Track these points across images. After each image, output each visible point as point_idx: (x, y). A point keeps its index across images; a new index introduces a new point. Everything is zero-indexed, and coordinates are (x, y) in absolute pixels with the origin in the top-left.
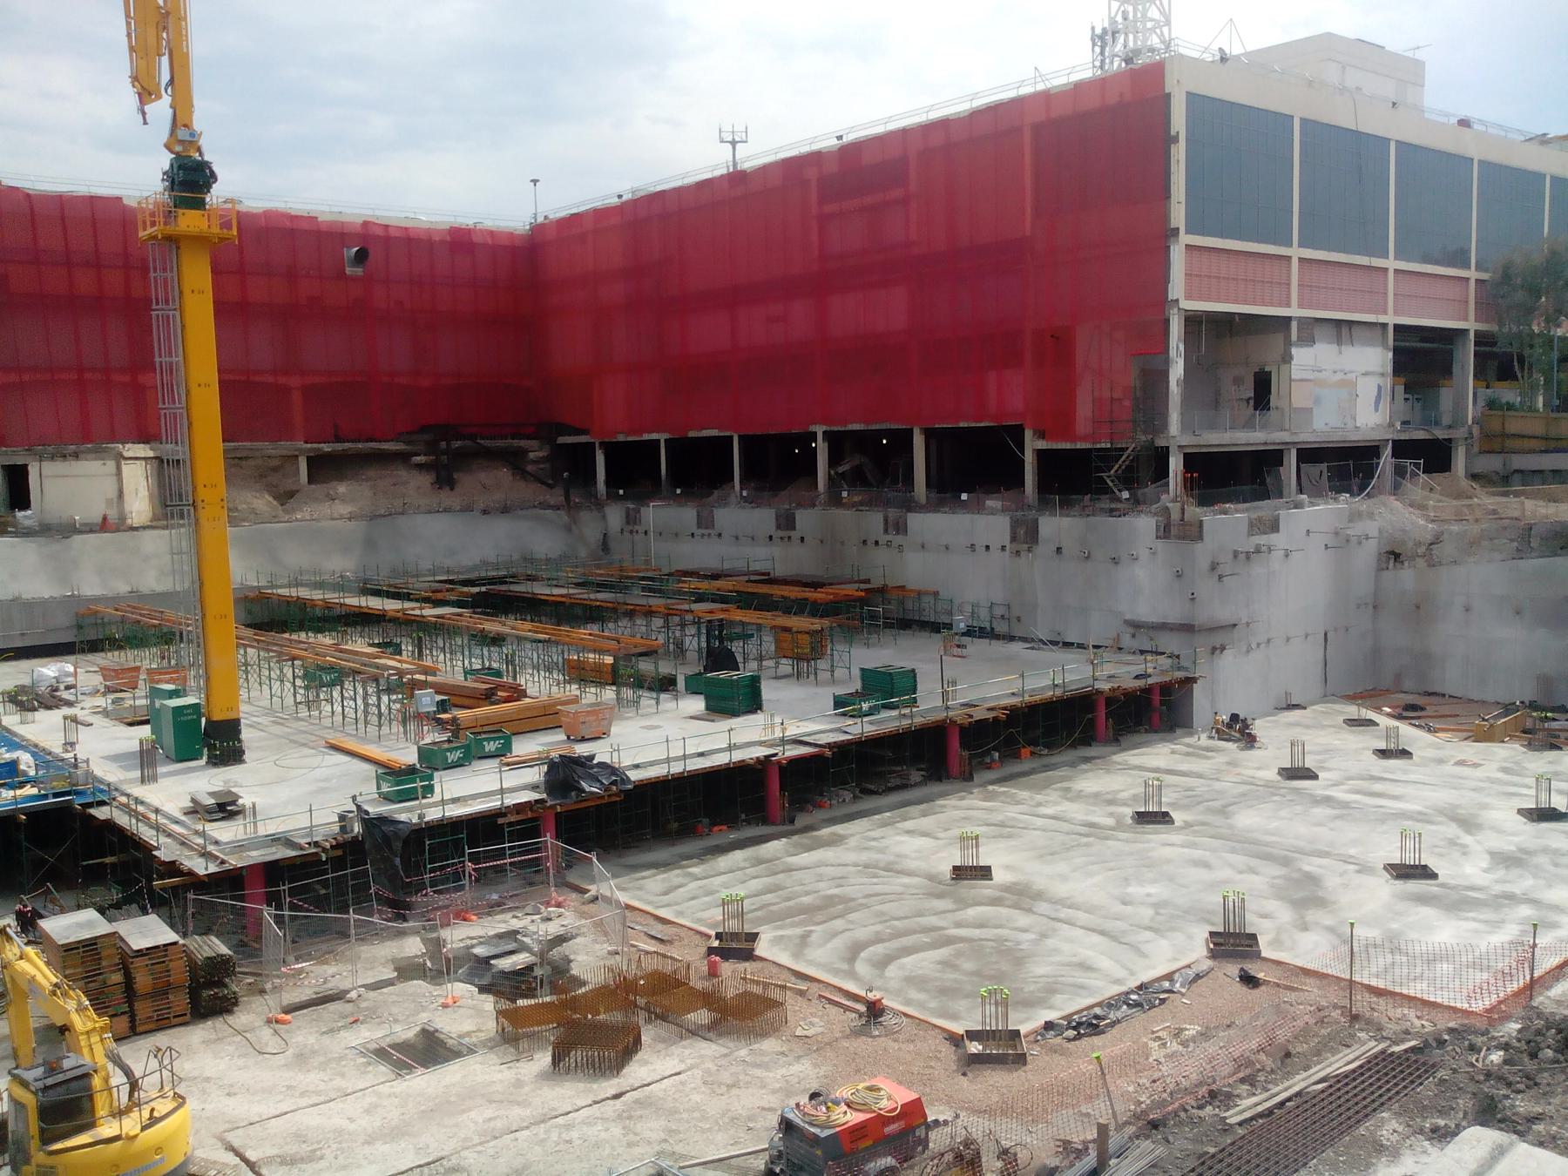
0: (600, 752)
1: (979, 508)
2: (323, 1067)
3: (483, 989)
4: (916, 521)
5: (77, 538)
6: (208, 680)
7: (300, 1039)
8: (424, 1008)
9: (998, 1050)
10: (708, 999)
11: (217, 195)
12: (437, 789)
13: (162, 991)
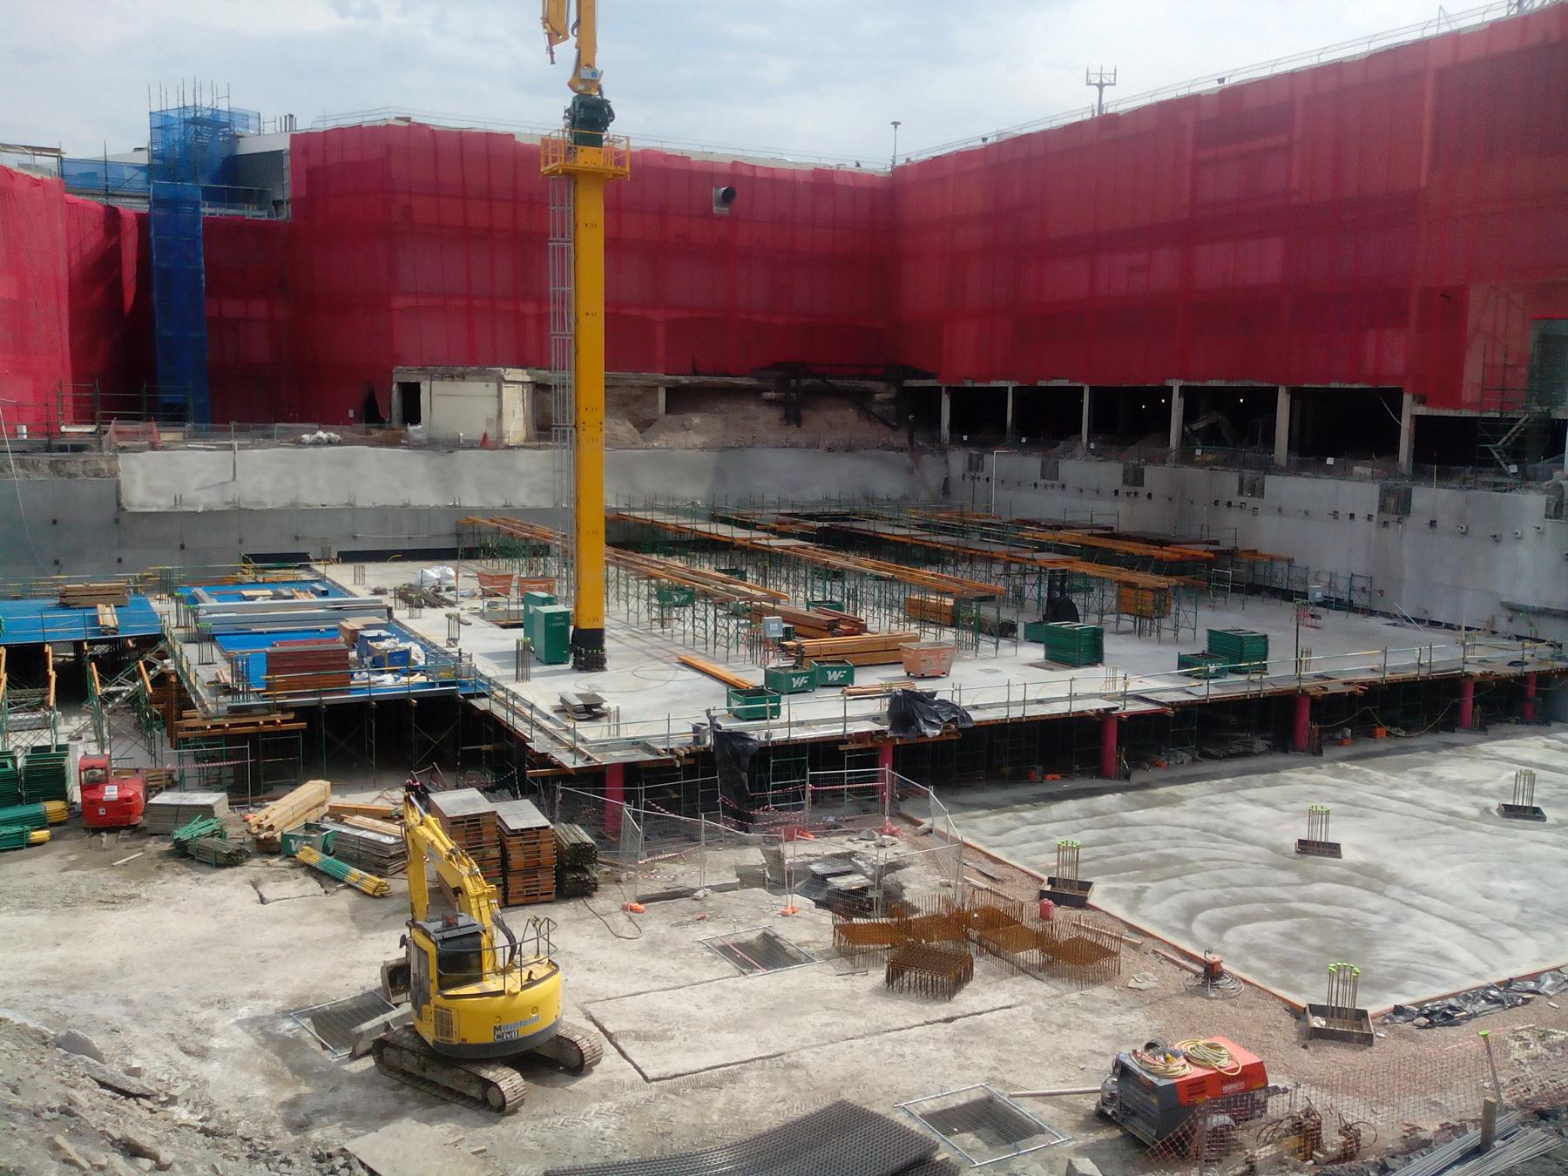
0: (942, 690)
1: (1345, 474)
2: (673, 955)
3: (819, 904)
4: (1273, 483)
5: (461, 453)
6: (578, 590)
7: (652, 927)
8: (765, 915)
9: (1343, 1027)
10: (1040, 940)
11: (614, 129)
12: (784, 711)
13: (532, 870)
